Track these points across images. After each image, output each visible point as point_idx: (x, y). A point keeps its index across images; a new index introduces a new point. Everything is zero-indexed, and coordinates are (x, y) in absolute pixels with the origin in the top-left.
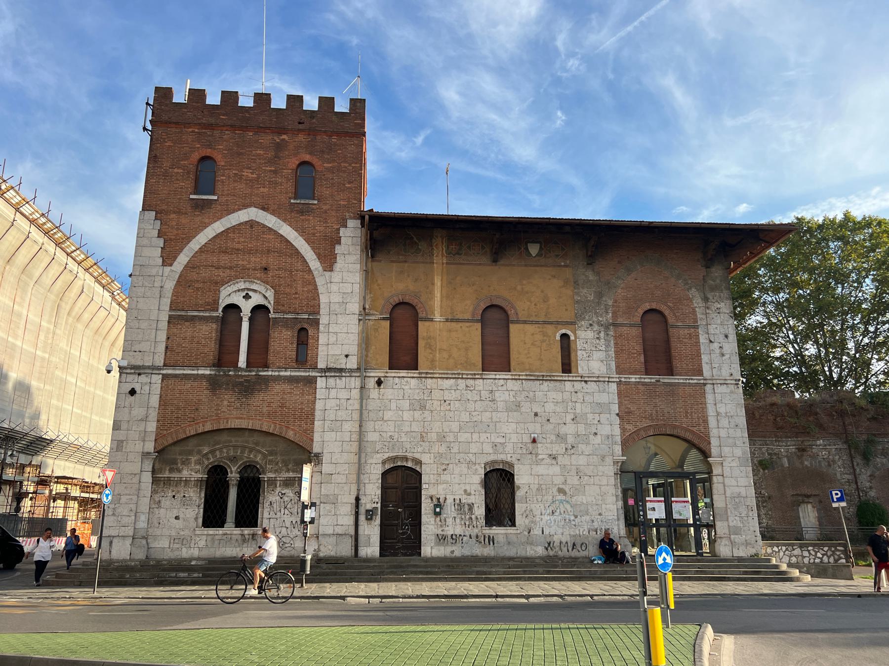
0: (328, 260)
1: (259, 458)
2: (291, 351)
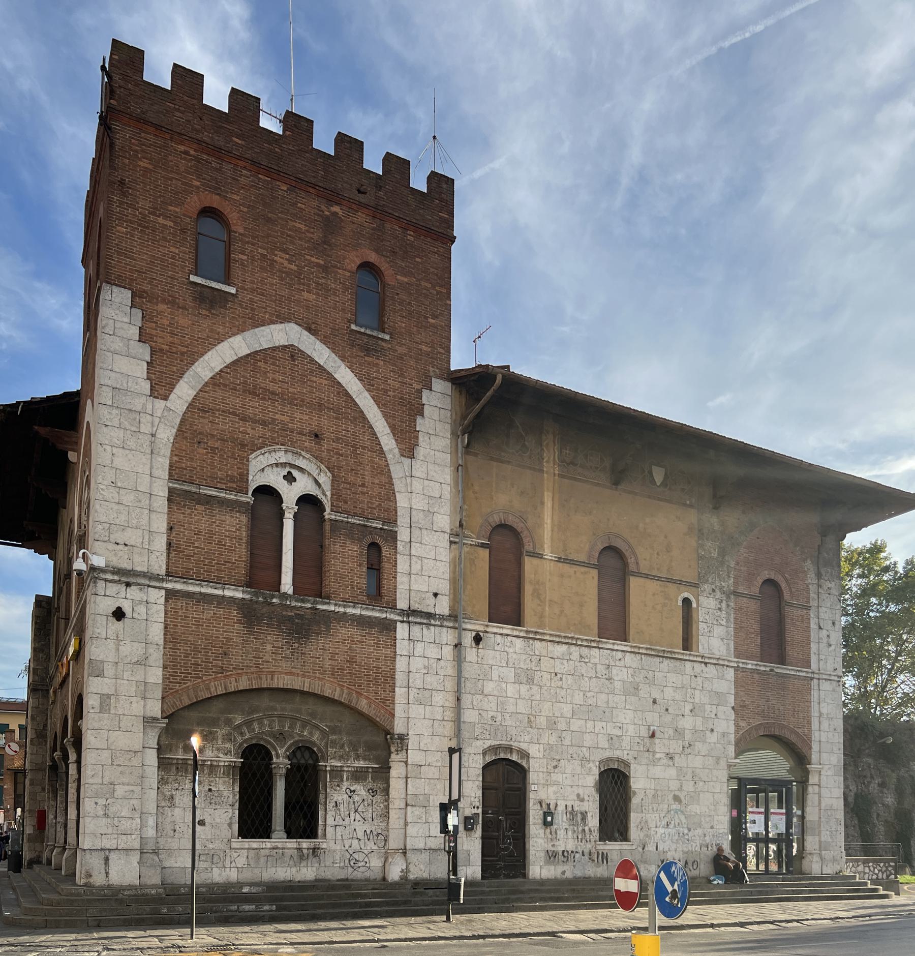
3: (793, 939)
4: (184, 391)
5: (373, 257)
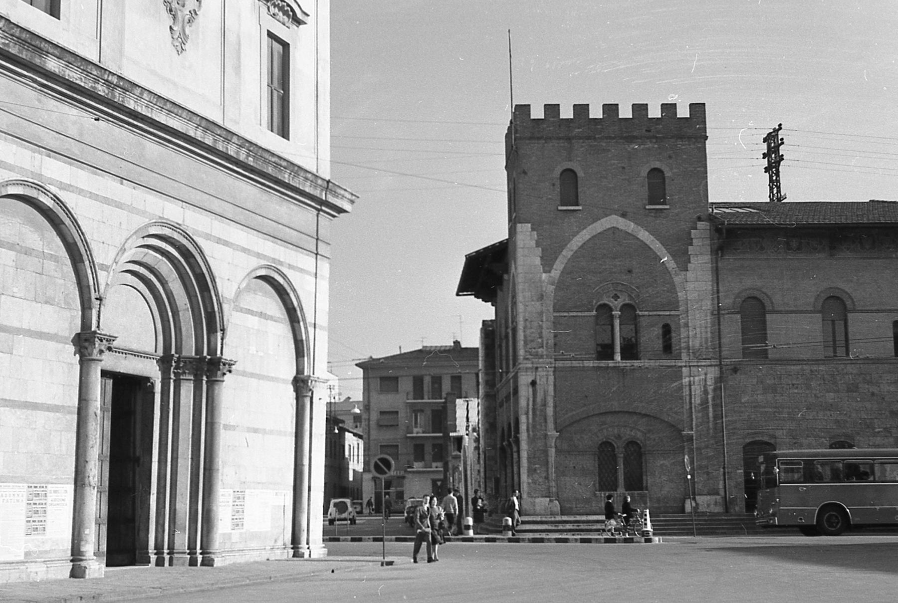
0: (683, 259)
1: (639, 434)
2: (659, 344)
3: (75, 89)
4: (559, 266)
5: (657, 165)
